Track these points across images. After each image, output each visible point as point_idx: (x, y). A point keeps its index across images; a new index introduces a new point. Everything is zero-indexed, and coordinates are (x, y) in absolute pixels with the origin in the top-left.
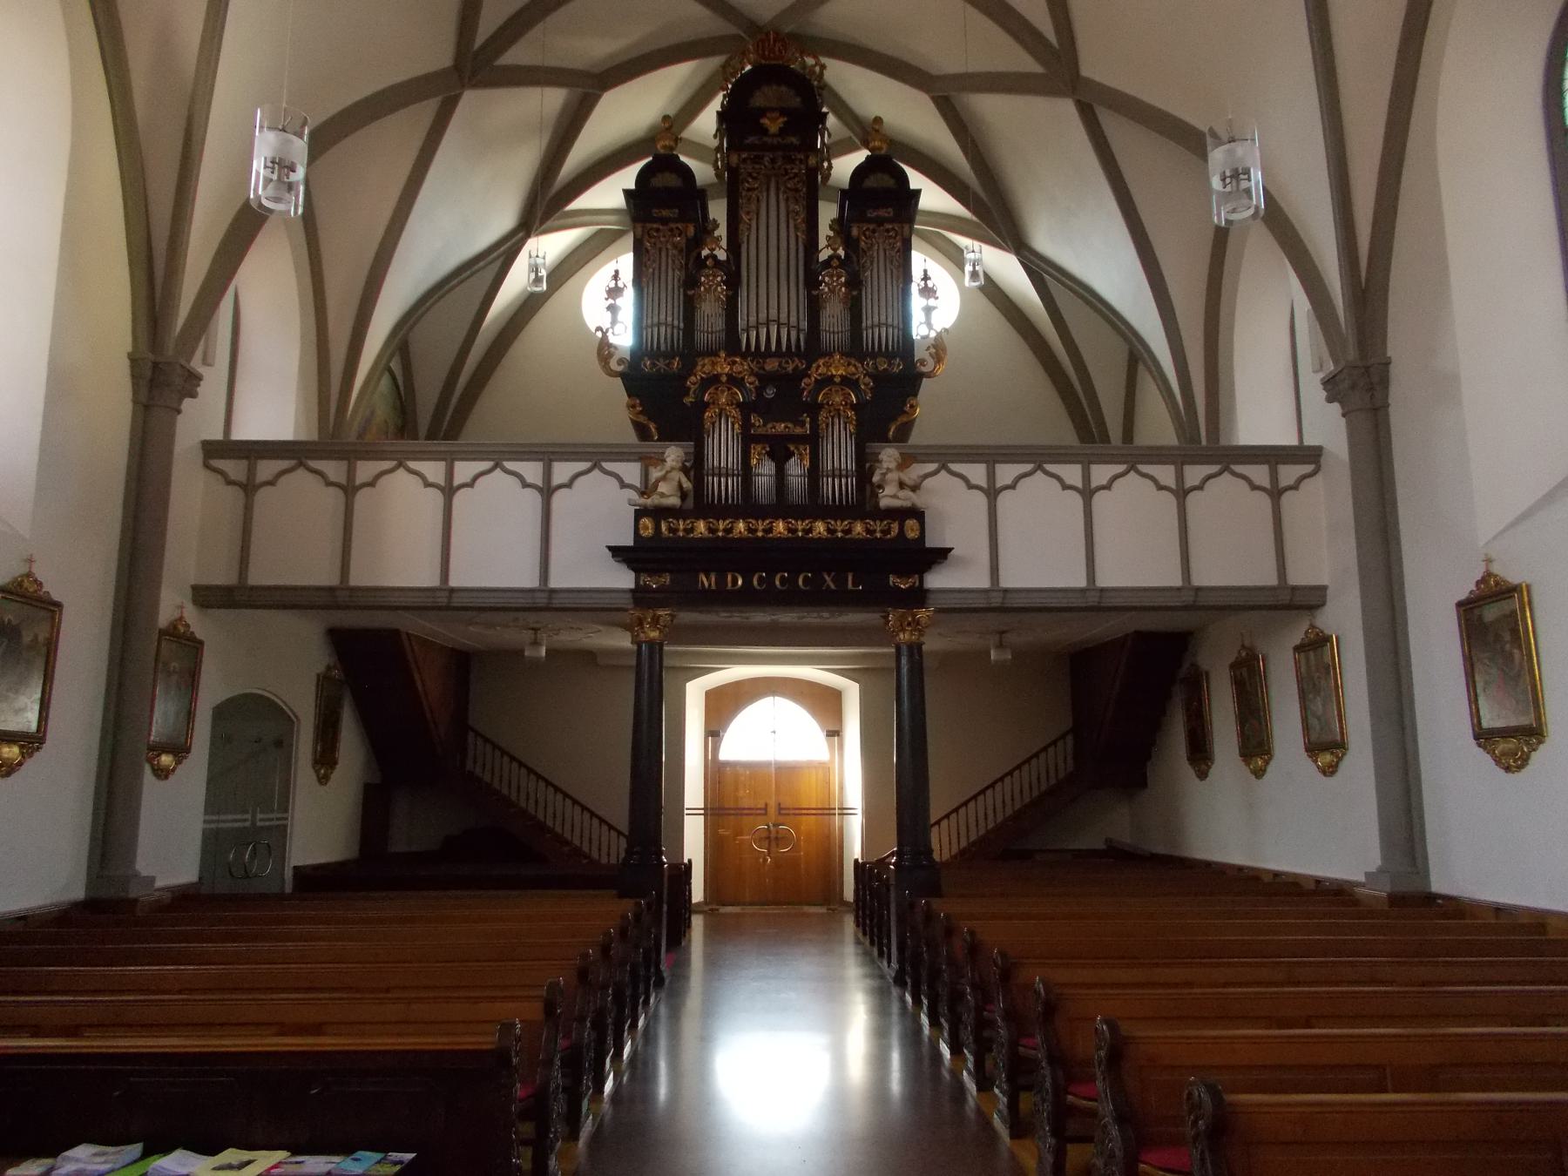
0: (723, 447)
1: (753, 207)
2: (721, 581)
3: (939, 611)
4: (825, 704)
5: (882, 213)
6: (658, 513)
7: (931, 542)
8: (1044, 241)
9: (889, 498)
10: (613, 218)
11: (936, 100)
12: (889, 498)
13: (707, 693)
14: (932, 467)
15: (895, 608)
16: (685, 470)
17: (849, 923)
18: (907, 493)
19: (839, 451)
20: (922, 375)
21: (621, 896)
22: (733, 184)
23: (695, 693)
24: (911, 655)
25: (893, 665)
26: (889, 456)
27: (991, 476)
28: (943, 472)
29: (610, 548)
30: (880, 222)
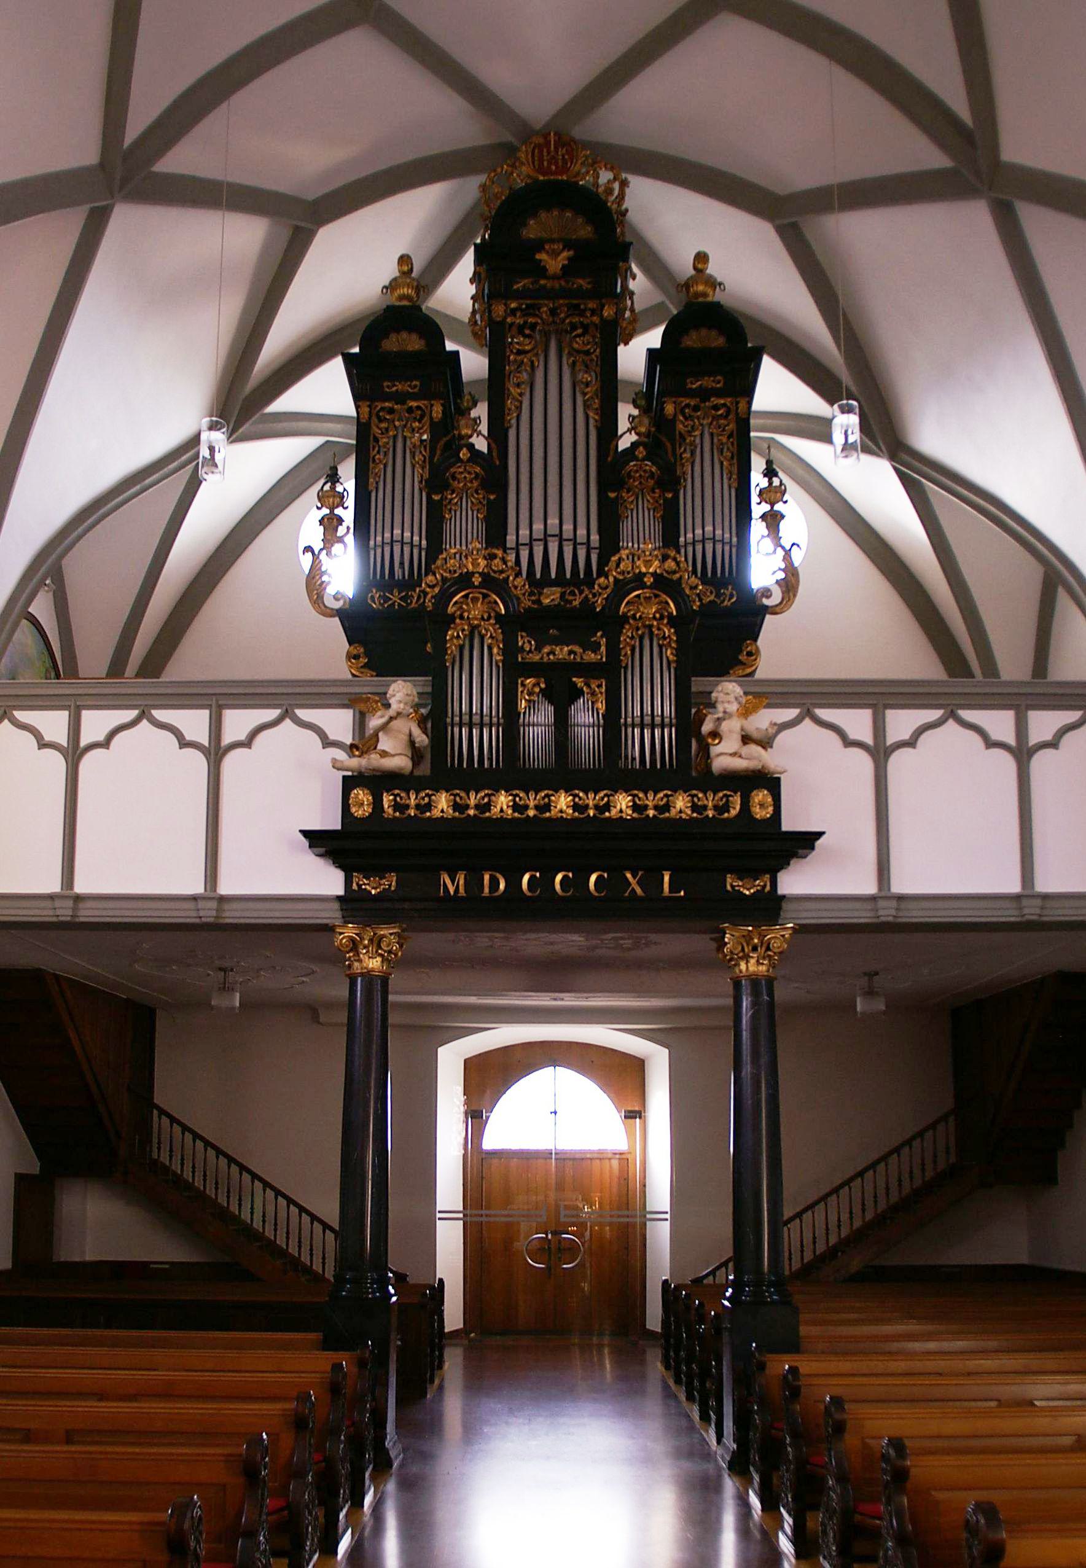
0: (476, 691)
1: (525, 376)
2: (474, 883)
3: (801, 930)
4: (622, 1076)
5: (708, 382)
6: (378, 782)
7: (789, 823)
8: (934, 436)
9: (727, 755)
10: (338, 427)
11: (781, 231)
12: (727, 755)
13: (465, 1061)
14: (792, 713)
15: (735, 924)
16: (422, 722)
17: (656, 1368)
18: (754, 749)
19: (651, 696)
20: (766, 610)
21: (328, 1344)
22: (493, 336)
23: (450, 1060)
24: (756, 992)
25: (730, 1001)
26: (728, 693)
27: (879, 728)
28: (807, 722)
29: (306, 833)
30: (704, 394)
